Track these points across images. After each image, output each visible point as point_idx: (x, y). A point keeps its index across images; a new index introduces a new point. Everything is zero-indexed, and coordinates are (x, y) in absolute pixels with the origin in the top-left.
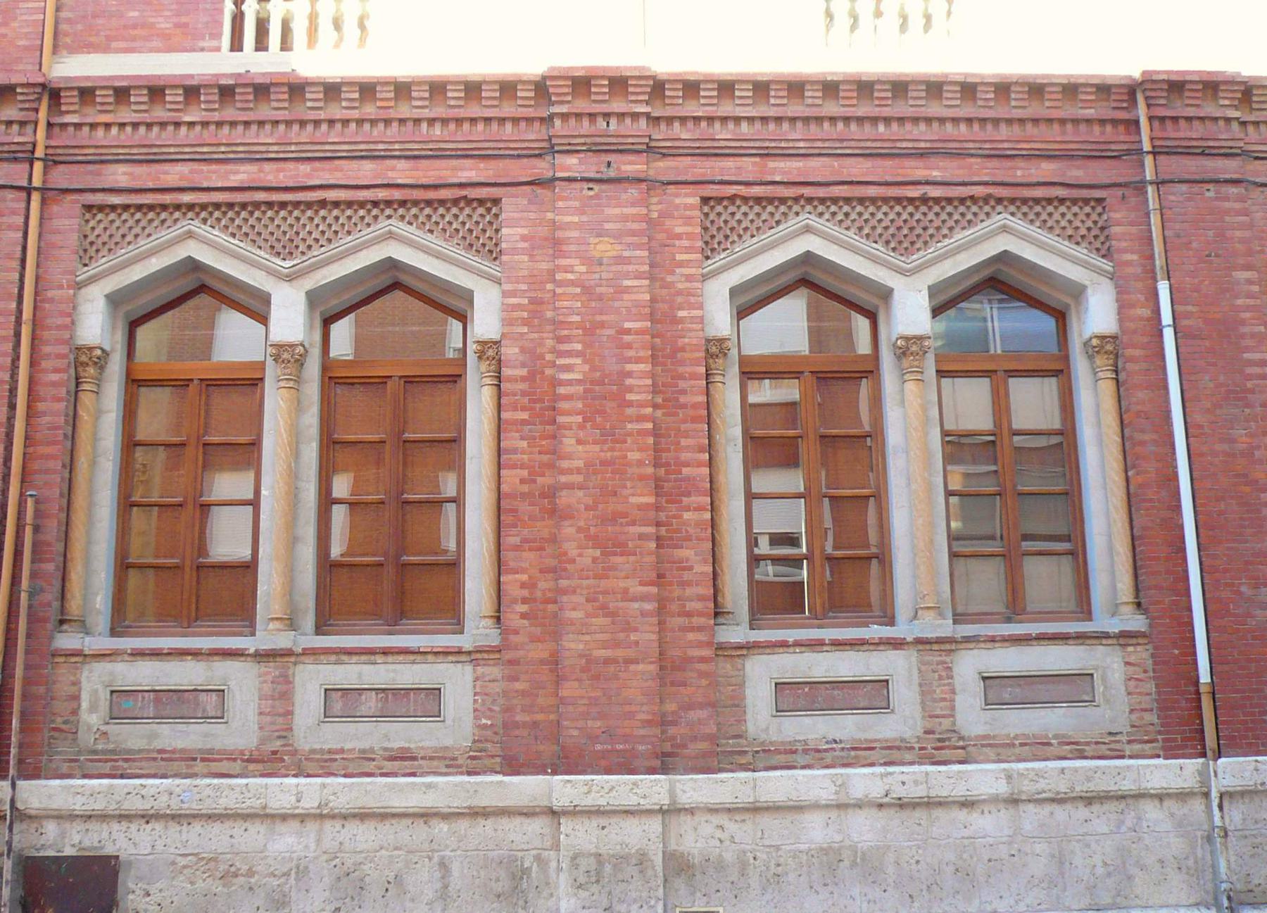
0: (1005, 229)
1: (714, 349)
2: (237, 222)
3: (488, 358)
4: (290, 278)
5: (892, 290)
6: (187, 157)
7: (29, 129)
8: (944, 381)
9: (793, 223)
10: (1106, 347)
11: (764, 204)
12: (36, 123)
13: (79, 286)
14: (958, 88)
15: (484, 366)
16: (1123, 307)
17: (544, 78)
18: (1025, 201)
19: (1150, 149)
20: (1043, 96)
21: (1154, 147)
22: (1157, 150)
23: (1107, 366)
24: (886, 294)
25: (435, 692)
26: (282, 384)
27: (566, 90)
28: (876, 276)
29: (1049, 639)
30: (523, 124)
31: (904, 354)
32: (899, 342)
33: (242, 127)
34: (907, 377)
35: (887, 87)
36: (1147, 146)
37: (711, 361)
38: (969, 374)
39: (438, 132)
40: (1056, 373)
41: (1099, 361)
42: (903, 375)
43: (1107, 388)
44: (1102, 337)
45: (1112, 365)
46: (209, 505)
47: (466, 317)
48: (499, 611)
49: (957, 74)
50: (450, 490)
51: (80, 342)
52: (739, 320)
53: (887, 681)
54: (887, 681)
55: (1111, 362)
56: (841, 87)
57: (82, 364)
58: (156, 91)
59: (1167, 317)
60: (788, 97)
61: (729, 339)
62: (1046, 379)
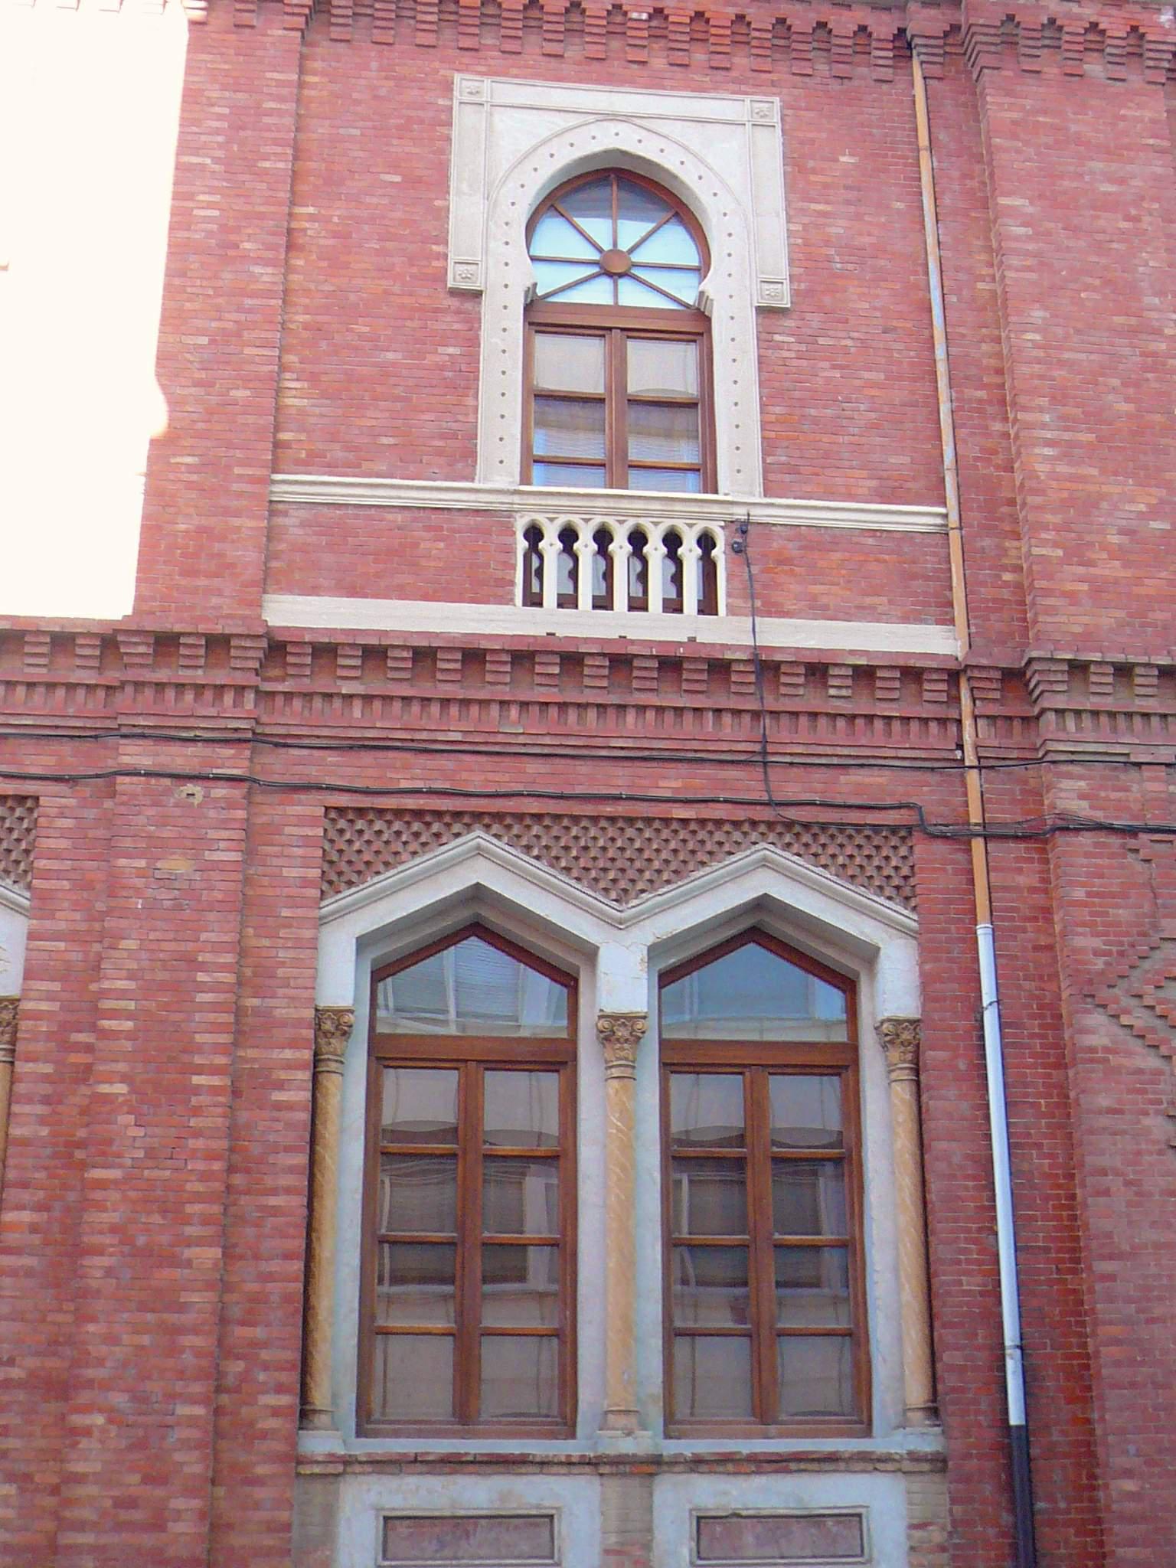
0: (765, 863)
1: (328, 1026)
2: (673, 845)
3: (902, 1043)
4: (618, 925)
5: (598, 948)
6: (823, 761)
7: (953, 728)
8: (675, 1079)
9: (453, 848)
10: (895, 1033)
11: (407, 819)
12: (959, 722)
13: (322, 922)
14: (459, 656)
15: (895, 1054)
16: (928, 985)
17: (116, 631)
18: (789, 825)
19: (975, 763)
20: (680, 675)
21: (979, 758)
22: (984, 763)
23: (904, 1061)
24: (590, 954)
25: (854, 1518)
26: (615, 1072)
27: (1059, 677)
28: (862, 933)
29: (819, 1460)
30: (377, 705)
31: (607, 1039)
32: (885, 1025)
33: (498, 707)
34: (894, 1076)
35: (405, 654)
36: (970, 759)
37: (322, 1041)
38: (808, 1070)
39: (357, 712)
40: (836, 1070)
41: (895, 1054)
42: (890, 1072)
43: (903, 1092)
44: (897, 1022)
45: (911, 1062)
46: (525, 1245)
47: (576, 980)
48: (934, 1400)
49: (586, 640)
50: (537, 1223)
51: (322, 1004)
52: (661, 987)
53: (551, 1517)
54: (551, 1517)
55: (909, 1056)
56: (685, 666)
57: (325, 1034)
58: (817, 670)
59: (988, 993)
60: (362, 667)
61: (352, 1012)
62: (825, 1078)
